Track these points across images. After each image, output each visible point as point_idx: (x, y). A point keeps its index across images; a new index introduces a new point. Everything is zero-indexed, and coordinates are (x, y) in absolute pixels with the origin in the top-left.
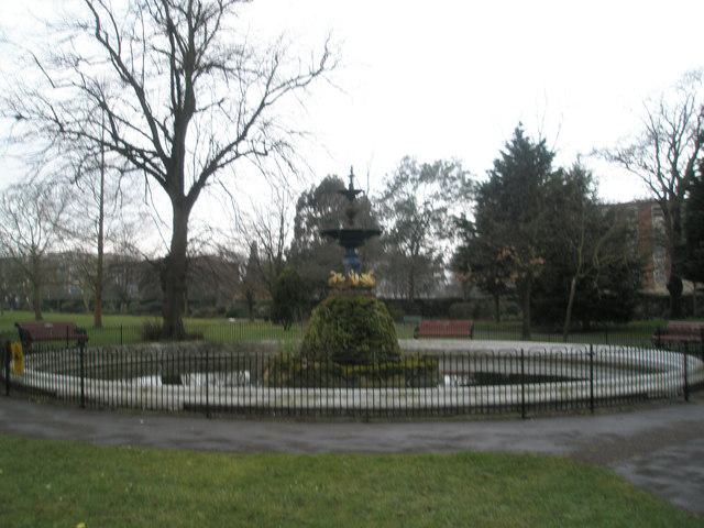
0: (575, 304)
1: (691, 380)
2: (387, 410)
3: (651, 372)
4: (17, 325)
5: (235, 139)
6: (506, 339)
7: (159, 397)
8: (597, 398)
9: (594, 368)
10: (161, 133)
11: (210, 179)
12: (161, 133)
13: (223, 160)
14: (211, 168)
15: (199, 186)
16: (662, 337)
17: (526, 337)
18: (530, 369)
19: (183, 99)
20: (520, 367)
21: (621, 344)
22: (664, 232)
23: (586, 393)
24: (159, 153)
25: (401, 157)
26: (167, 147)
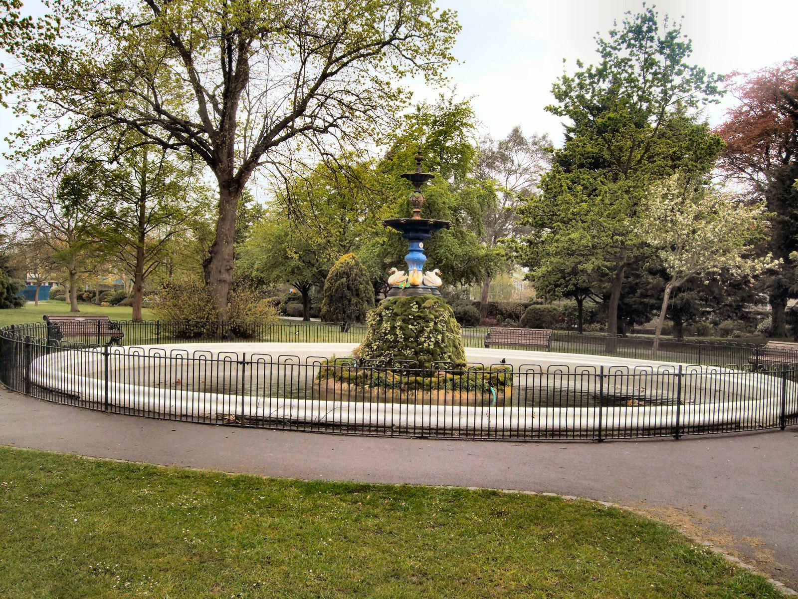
0: (669, 307)
1: (790, 409)
2: (661, 428)
3: (662, 404)
4: (45, 318)
5: (71, 112)
6: (586, 352)
7: (208, 406)
8: (606, 429)
9: (103, 401)
10: (209, 107)
11: (263, 158)
12: (209, 107)
13: (277, 137)
14: (266, 143)
15: (250, 165)
16: (760, 358)
17: (610, 351)
18: (610, 388)
19: (234, 64)
20: (598, 386)
21: (732, 367)
22: (213, 229)
23: (671, 420)
24: (206, 126)
25: (532, 135)
26: (214, 118)
